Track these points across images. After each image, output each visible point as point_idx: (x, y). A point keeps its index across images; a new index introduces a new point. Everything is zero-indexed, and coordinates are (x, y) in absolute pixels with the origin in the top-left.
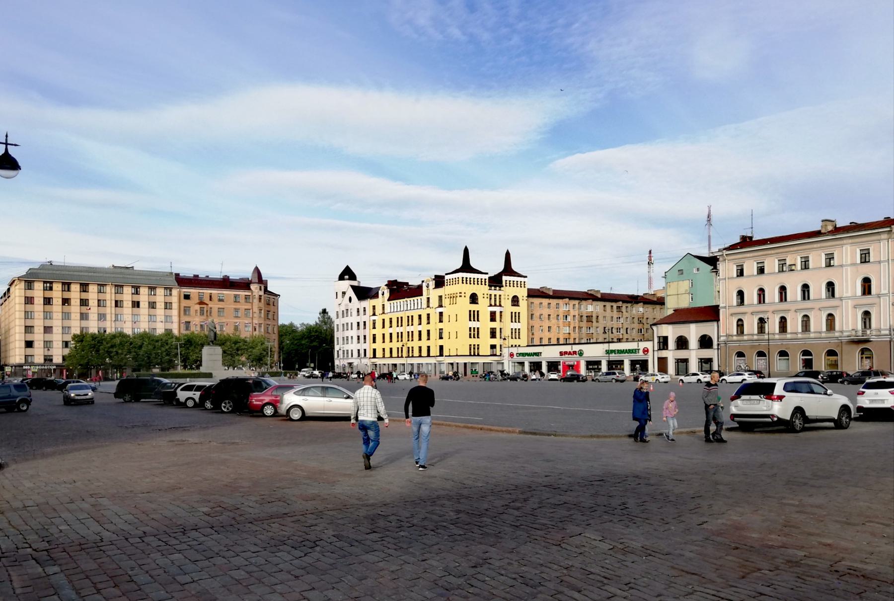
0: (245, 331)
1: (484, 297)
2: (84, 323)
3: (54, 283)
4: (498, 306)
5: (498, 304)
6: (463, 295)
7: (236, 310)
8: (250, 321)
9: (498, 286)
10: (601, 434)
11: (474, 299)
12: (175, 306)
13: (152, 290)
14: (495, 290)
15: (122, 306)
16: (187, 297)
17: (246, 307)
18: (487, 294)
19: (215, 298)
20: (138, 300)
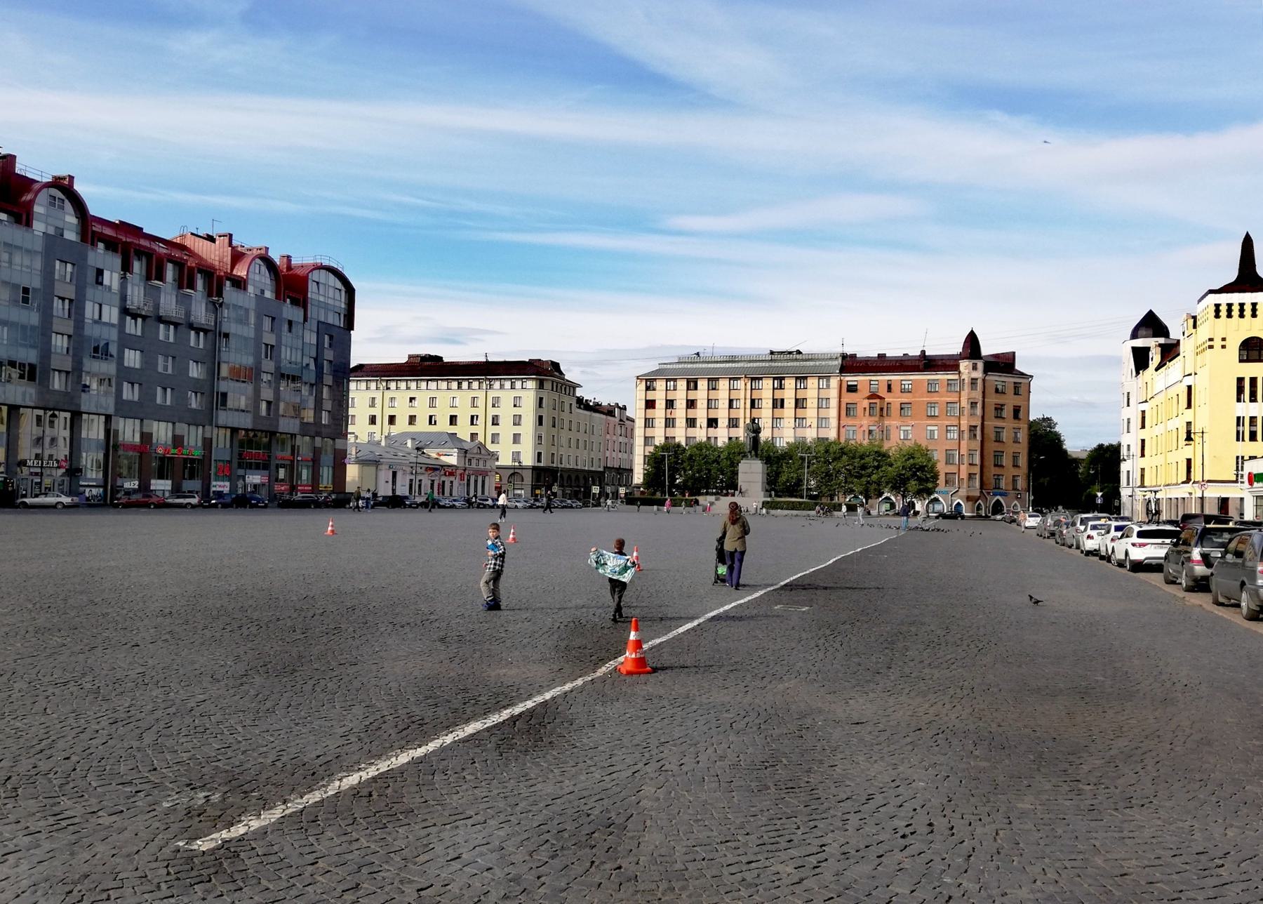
2: (670, 432)
6: (1217, 343)
7: (932, 405)
8: (956, 423)
10: (829, 585)
12: (834, 403)
14: (408, 388)
16: (852, 389)
17: (949, 400)
19: (895, 388)
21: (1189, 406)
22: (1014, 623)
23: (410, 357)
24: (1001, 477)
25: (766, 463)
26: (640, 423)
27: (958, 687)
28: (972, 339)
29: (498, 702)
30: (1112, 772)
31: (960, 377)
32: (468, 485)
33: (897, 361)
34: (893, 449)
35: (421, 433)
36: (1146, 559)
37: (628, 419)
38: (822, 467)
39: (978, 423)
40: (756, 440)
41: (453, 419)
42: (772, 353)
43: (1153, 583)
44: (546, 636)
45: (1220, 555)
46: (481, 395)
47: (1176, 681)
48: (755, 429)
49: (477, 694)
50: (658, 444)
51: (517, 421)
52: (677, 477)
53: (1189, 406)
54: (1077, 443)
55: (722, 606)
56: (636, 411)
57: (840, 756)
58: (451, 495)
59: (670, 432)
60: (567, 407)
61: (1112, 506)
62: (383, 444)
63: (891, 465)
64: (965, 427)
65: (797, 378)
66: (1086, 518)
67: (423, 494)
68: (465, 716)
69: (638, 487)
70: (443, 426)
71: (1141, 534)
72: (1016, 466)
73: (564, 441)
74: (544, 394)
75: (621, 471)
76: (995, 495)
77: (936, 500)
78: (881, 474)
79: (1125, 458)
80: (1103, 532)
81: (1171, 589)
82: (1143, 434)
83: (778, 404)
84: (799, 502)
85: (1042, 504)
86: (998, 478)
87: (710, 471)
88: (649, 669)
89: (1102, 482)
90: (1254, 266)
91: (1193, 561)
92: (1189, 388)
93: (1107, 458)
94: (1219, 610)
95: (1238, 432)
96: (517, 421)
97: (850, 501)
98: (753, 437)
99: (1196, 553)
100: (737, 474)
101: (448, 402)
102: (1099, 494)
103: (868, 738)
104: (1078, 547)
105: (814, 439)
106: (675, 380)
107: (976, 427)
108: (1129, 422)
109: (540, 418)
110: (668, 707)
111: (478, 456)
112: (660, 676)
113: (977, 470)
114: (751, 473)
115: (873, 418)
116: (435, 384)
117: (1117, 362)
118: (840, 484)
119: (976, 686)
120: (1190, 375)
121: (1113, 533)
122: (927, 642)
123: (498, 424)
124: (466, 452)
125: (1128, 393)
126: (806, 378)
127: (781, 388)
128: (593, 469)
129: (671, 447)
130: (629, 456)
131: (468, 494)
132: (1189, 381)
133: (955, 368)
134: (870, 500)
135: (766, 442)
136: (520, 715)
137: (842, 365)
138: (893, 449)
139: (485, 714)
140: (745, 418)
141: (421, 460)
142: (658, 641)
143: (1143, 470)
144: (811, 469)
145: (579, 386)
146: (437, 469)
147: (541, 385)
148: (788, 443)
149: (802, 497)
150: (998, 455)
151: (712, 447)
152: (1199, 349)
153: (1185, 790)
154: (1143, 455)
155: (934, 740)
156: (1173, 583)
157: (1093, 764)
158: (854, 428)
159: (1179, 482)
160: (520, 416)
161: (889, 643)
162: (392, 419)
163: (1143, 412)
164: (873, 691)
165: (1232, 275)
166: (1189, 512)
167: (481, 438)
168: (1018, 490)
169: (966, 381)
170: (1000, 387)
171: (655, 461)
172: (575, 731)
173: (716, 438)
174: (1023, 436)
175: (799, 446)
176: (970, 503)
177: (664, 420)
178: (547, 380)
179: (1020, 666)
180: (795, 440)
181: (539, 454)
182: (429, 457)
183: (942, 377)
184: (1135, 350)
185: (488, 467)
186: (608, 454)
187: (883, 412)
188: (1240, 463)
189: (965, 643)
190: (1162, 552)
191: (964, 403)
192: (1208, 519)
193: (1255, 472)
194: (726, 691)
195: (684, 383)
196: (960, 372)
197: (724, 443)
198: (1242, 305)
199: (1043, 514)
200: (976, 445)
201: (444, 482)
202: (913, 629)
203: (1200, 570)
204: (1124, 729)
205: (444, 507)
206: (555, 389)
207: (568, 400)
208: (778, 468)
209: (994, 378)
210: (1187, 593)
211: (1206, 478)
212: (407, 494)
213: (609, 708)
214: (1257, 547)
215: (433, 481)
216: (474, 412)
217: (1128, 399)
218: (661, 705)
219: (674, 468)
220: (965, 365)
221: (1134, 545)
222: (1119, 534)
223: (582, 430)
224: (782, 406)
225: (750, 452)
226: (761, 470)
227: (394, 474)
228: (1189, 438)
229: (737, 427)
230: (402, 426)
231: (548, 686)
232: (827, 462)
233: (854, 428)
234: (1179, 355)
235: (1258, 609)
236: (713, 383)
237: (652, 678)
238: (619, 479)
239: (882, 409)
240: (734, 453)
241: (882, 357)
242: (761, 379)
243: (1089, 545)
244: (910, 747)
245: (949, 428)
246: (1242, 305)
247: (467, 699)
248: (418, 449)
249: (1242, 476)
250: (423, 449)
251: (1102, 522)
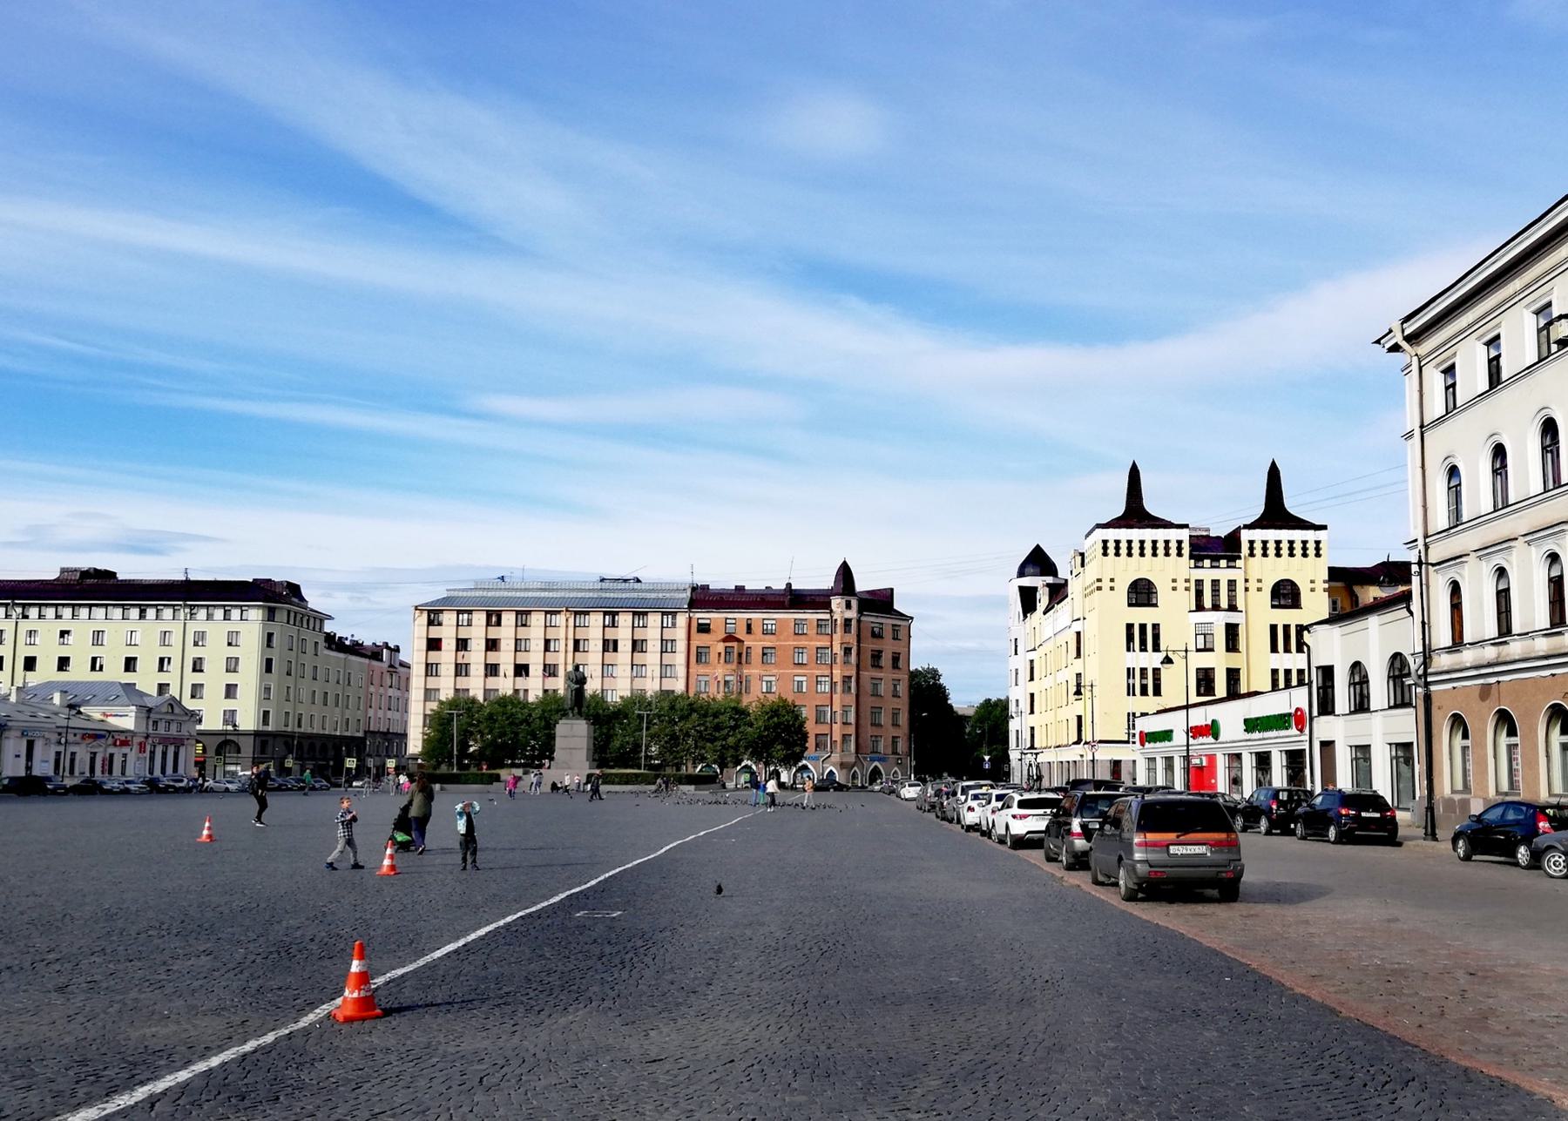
0: (817, 692)
1: (1174, 589)
2: (463, 683)
4: (1208, 610)
5: (1224, 603)
6: (1106, 584)
7: (800, 650)
8: (827, 672)
9: (1207, 557)
11: (1142, 593)
12: (681, 646)
13: (641, 617)
14: (58, 617)
15: (644, 650)
16: (704, 629)
17: (819, 644)
18: (1187, 581)
19: (756, 628)
20: (615, 638)
21: (1079, 655)
22: (871, 917)
23: (63, 571)
24: (879, 739)
25: (592, 724)
26: (418, 671)
27: (789, 1002)
28: (845, 573)
29: (133, 1076)
30: (948, 1094)
31: (832, 617)
32: (152, 759)
33: (758, 595)
34: (754, 704)
35: (77, 683)
36: (1029, 832)
37: (402, 664)
38: (666, 727)
39: (853, 673)
40: (579, 693)
41: (130, 664)
42: (603, 580)
43: (1033, 862)
44: (231, 974)
45: (1098, 827)
46: (176, 628)
47: (1036, 977)
48: (578, 679)
49: (101, 1067)
50: (443, 698)
51: (232, 665)
52: (471, 743)
53: (1079, 655)
54: (963, 699)
55: (504, 917)
56: (414, 654)
57: (622, 1107)
58: (123, 774)
59: (463, 683)
60: (310, 648)
61: (999, 773)
62: (13, 699)
63: (751, 725)
64: (837, 678)
65: (634, 613)
66: (967, 786)
67: (77, 773)
68: (75, 1101)
69: (414, 758)
70: (114, 672)
71: (1022, 804)
72: (895, 725)
73: (305, 695)
74: (275, 628)
75: (390, 736)
76: (873, 760)
77: (805, 768)
78: (739, 736)
79: (1014, 715)
80: (984, 802)
81: (1051, 868)
82: (1033, 687)
83: (610, 646)
84: (635, 774)
85: (925, 770)
86: (876, 739)
87: (517, 734)
88: (378, 1011)
89: (989, 745)
90: (1141, 499)
91: (1073, 834)
92: (1078, 634)
93: (995, 715)
94: (1100, 893)
95: (1129, 685)
96: (232, 665)
97: (701, 770)
98: (576, 689)
99: (1076, 825)
100: (554, 738)
101: (123, 638)
102: (987, 758)
103: (662, 1079)
104: (959, 821)
105: (656, 693)
106: (470, 612)
107: (850, 677)
108: (1017, 674)
109: (269, 663)
110: (395, 1063)
111: (169, 717)
112: (395, 1020)
113: (851, 730)
114: (573, 736)
115: (729, 666)
116: (103, 610)
117: (1003, 603)
118: (688, 750)
119: (810, 1000)
120: (1079, 619)
121: (995, 804)
122: (761, 948)
123: (202, 671)
124: (150, 710)
125: (1016, 639)
126: (529, 612)
127: (613, 626)
128: (348, 734)
129: (462, 703)
130: (402, 715)
131: (151, 772)
132: (1077, 627)
133: (826, 605)
134: (725, 770)
135: (594, 696)
136: (164, 1093)
137: (691, 598)
138: (754, 704)
139: (107, 1095)
140: (566, 664)
141: (75, 722)
142: (400, 972)
143: (1032, 728)
144: (652, 731)
145: (330, 618)
146: (103, 736)
147: (271, 615)
148: (621, 697)
149: (640, 768)
150: (876, 711)
151: (520, 703)
152: (1088, 591)
153: (1025, 1108)
154: (1032, 712)
155: (747, 1073)
156: (1055, 860)
157: (930, 1086)
158: (706, 679)
159: (1070, 743)
160: (237, 659)
161: (715, 952)
162: (30, 663)
163: (1032, 661)
164: (683, 1016)
165: (1119, 509)
166: (1081, 778)
167: (174, 691)
168: (899, 754)
169: (839, 622)
170: (876, 630)
171: (439, 723)
172: (245, 1109)
173: (526, 691)
174: (903, 689)
175: (637, 700)
176: (845, 771)
177: (453, 666)
178: (279, 608)
179: (866, 971)
180: (632, 693)
181: (266, 714)
182: (89, 719)
183: (812, 616)
184: (1022, 589)
185: (184, 732)
186: (371, 713)
187: (742, 658)
188: (1131, 720)
189: (808, 945)
190: (1041, 825)
191: (837, 649)
192: (1098, 784)
193: (1146, 731)
194: (485, 1034)
195: (483, 616)
196: (831, 611)
197: (537, 697)
198: (1265, 543)
199: (924, 782)
200: (851, 699)
201: (112, 756)
202: (748, 932)
203: (1080, 844)
204: (971, 1040)
205: (110, 792)
206: (292, 622)
207: (311, 637)
208: (609, 730)
209: (870, 619)
210: (1067, 872)
211: (1097, 738)
212: (51, 773)
213: (306, 1071)
214: (1133, 815)
215: (95, 754)
216: (164, 652)
217: (1016, 646)
218: (385, 1061)
219: (466, 731)
220: (837, 603)
221: (1014, 817)
222: (1000, 804)
223: (333, 679)
224: (615, 650)
225: (572, 709)
226: (585, 733)
227: (30, 746)
228: (1078, 693)
229: (555, 676)
230: (46, 671)
231: (219, 1046)
232: (672, 722)
233: (706, 679)
234: (1067, 596)
235: (1136, 888)
236: (522, 616)
237: (381, 1025)
238: (387, 747)
239: (740, 655)
240: (550, 711)
241: (740, 589)
242: (587, 613)
243: (970, 818)
244: (715, 1086)
245: (819, 679)
246: (1265, 543)
247: (83, 1076)
248: (71, 707)
249: (1134, 735)
250: (80, 706)
251: (984, 790)
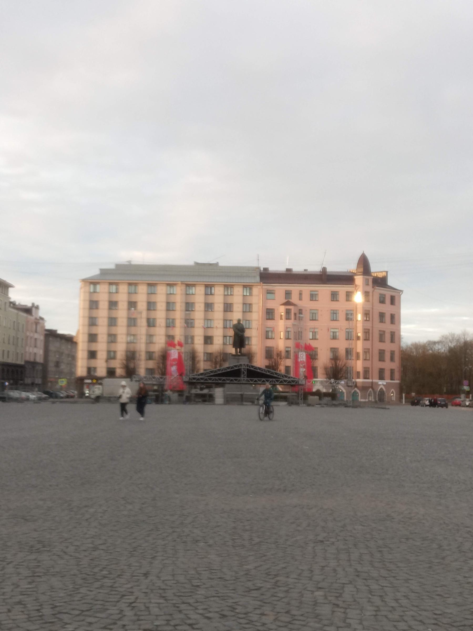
3: (197, 285)
